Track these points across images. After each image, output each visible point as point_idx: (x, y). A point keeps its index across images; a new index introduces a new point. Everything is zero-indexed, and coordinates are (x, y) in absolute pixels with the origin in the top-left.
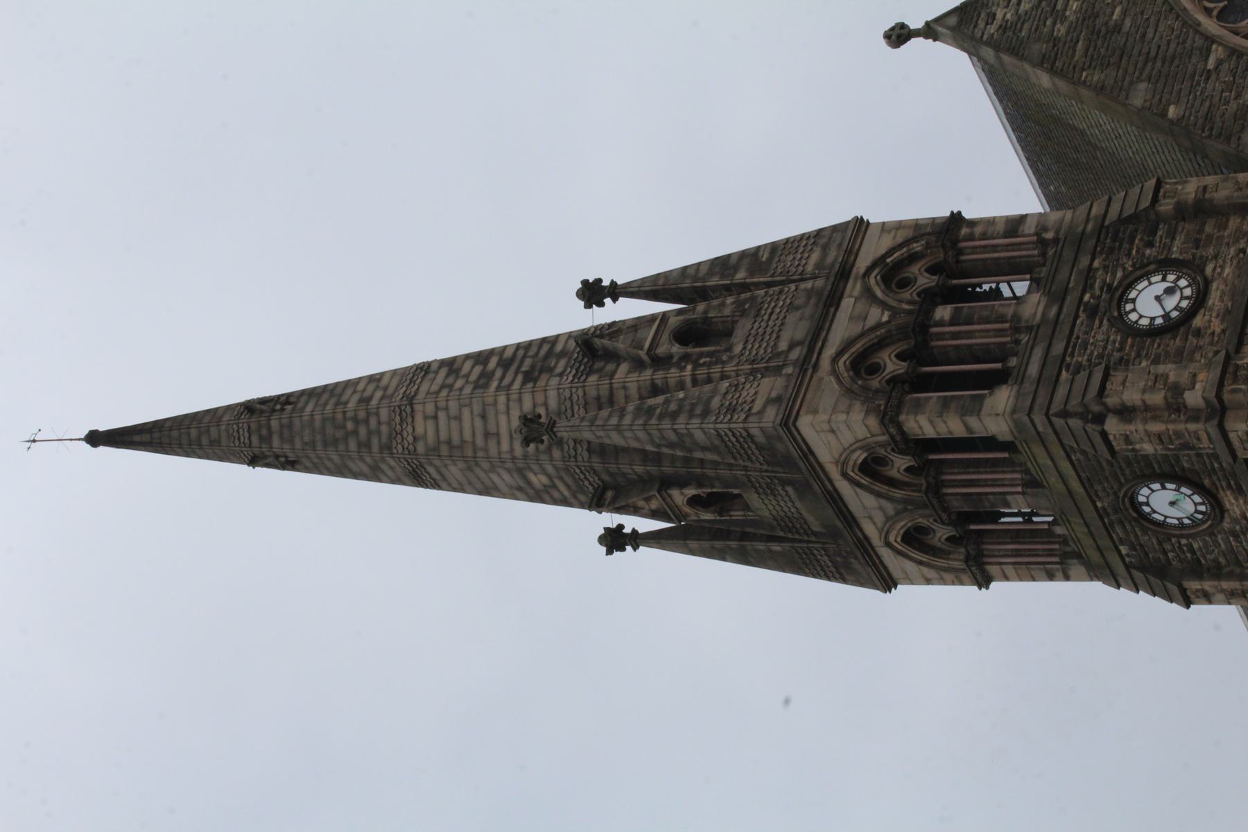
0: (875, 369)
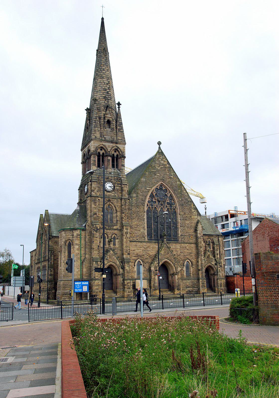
0: (101, 150)
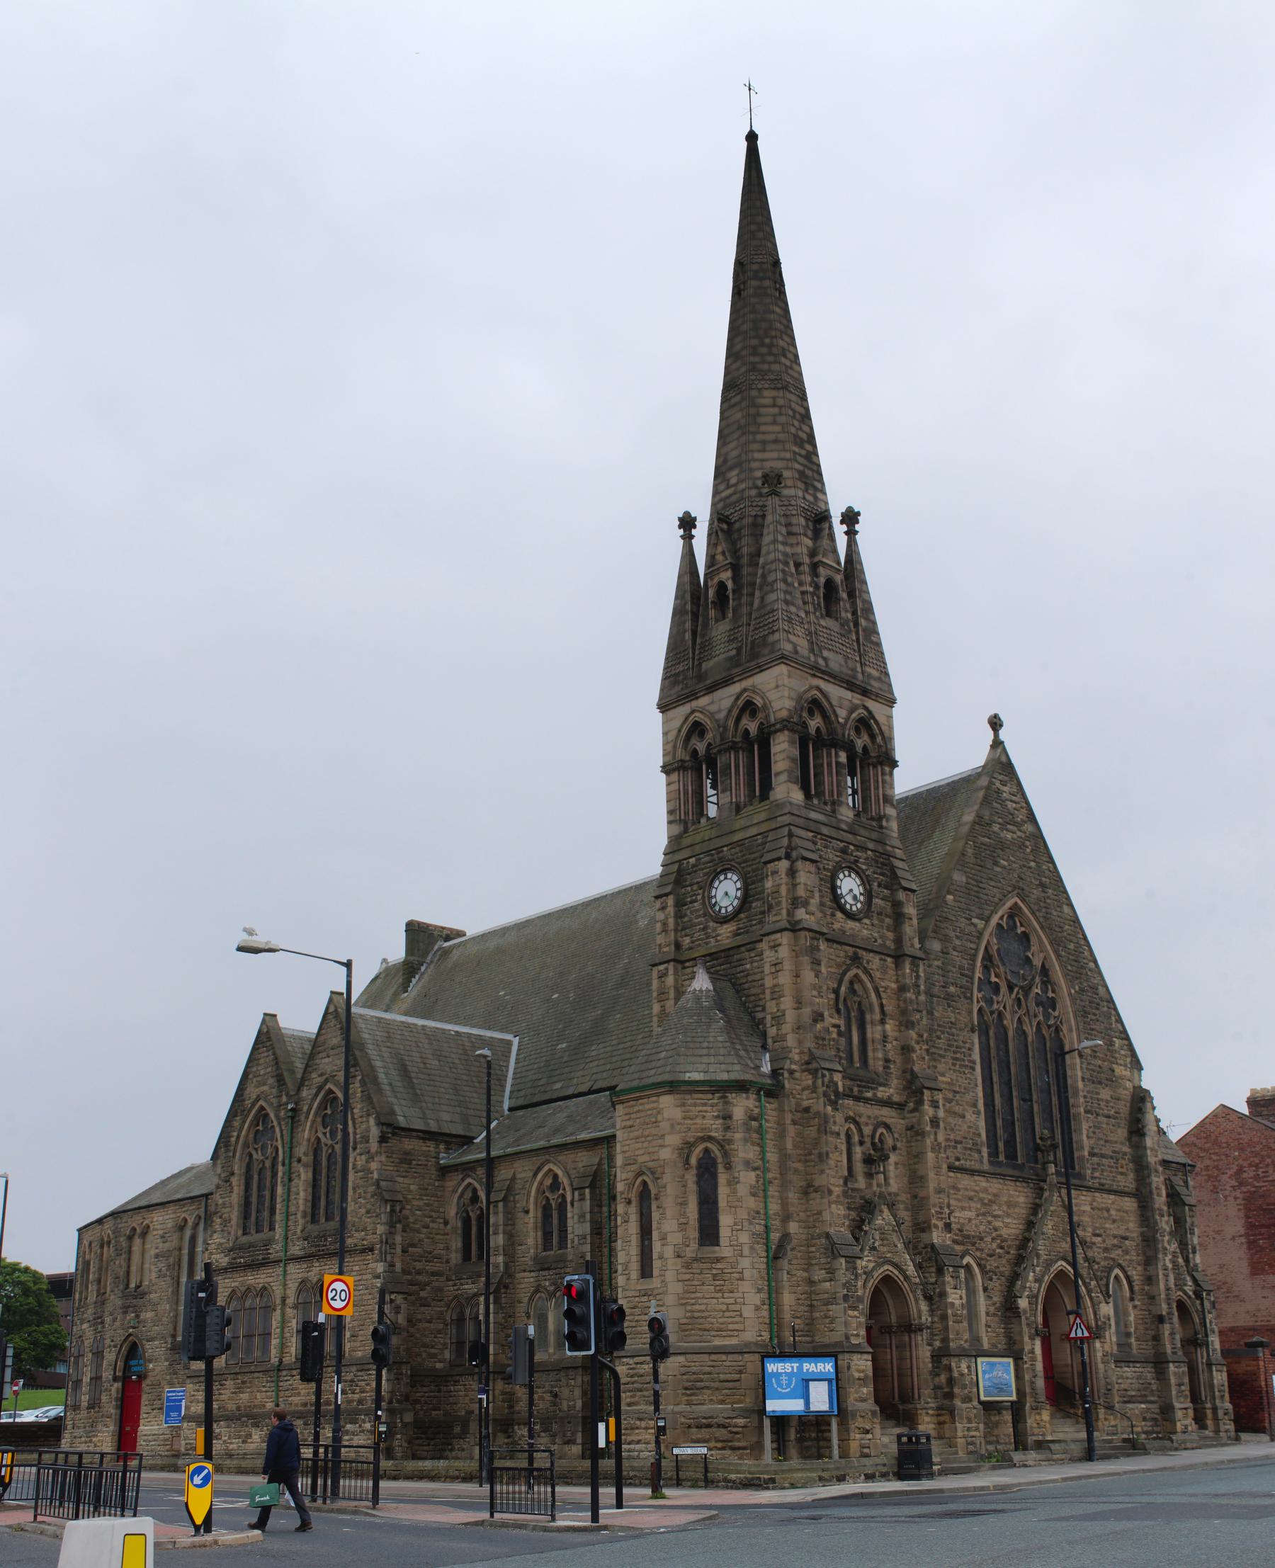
0: (811, 713)
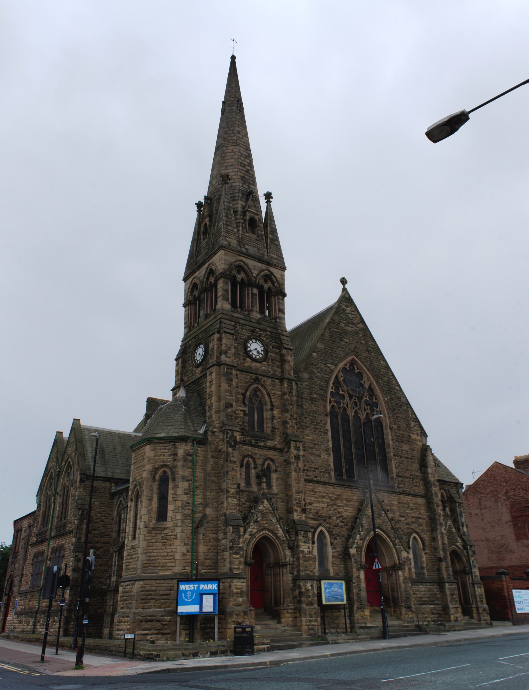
0: (239, 272)
